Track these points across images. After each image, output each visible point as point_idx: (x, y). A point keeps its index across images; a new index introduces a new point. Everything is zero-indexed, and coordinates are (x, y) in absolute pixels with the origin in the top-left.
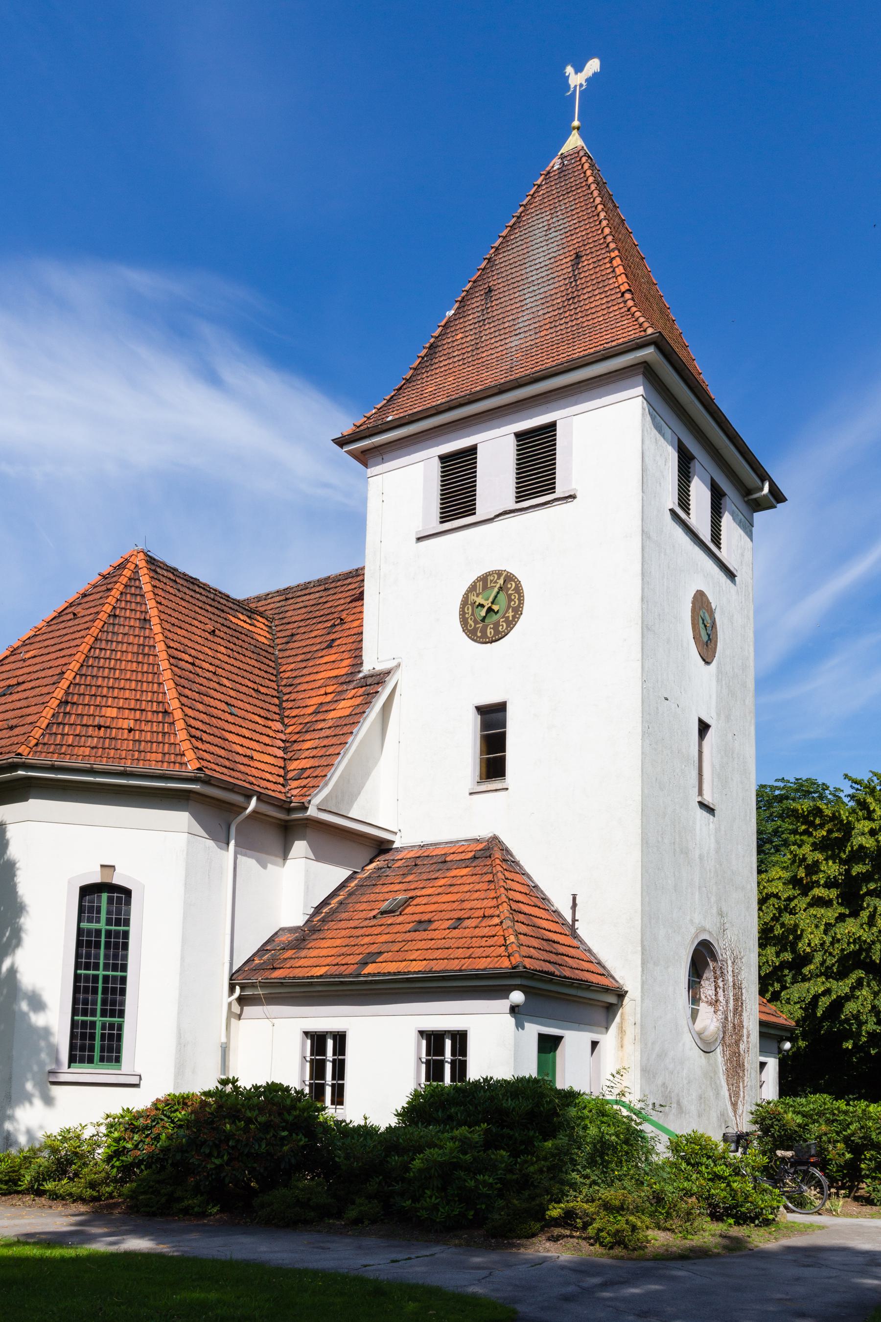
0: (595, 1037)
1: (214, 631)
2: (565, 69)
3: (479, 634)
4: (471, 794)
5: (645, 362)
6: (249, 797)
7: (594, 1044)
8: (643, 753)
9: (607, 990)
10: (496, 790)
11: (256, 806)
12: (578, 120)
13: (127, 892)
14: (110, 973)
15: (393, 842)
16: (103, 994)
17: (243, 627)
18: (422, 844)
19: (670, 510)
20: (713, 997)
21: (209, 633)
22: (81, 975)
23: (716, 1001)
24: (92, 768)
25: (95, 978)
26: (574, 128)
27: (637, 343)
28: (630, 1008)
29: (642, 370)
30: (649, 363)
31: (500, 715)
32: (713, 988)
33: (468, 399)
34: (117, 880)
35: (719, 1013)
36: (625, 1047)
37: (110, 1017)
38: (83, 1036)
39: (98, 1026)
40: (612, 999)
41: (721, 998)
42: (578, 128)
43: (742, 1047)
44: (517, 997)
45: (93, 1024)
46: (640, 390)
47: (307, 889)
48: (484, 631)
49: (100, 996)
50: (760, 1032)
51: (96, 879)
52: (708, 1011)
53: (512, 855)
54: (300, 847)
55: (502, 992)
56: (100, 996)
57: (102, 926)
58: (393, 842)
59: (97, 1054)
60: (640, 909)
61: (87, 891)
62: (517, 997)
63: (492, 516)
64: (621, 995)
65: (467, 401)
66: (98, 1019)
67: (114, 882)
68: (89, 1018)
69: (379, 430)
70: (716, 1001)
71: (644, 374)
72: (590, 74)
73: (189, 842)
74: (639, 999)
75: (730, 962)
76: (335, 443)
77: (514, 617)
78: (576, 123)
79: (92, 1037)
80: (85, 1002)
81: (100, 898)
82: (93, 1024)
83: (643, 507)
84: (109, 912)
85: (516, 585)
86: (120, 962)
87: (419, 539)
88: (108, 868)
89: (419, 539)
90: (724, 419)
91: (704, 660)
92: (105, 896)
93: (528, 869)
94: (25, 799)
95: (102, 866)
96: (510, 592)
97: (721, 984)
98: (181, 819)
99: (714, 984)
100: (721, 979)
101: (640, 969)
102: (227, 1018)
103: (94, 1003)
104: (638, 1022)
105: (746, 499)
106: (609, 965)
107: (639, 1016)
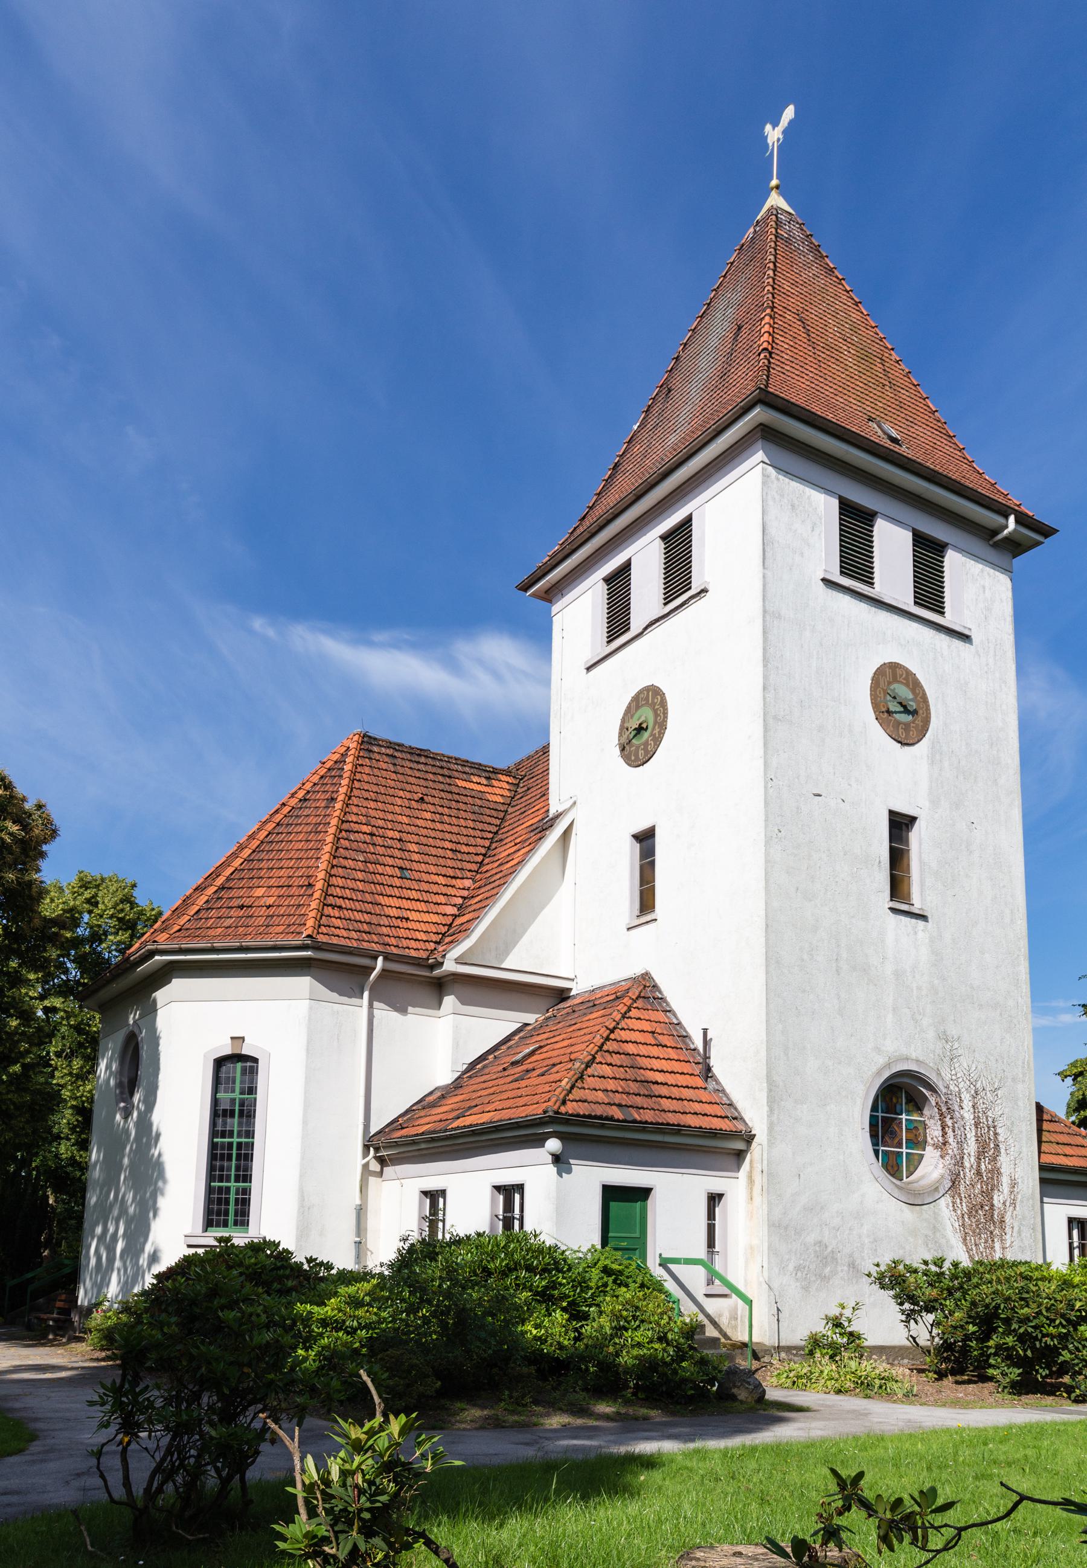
0: (716, 1189)
1: (422, 799)
2: (764, 129)
3: (633, 758)
4: (628, 929)
5: (761, 424)
6: (376, 958)
7: (714, 1199)
8: (767, 861)
9: (734, 1135)
10: (647, 922)
11: (383, 965)
12: (777, 178)
13: (255, 1060)
14: (243, 1140)
15: (570, 990)
16: (236, 1160)
17: (465, 788)
18: (592, 989)
19: (823, 580)
20: (940, 1139)
21: (417, 801)
22: (217, 1143)
23: (944, 1144)
24: (181, 948)
25: (230, 1144)
26: (772, 189)
27: (742, 408)
28: (756, 1153)
29: (759, 434)
30: (766, 423)
31: (649, 841)
32: (940, 1128)
33: (612, 513)
34: (245, 1051)
35: (948, 1157)
36: (754, 1199)
37: (243, 1182)
38: (219, 1201)
39: (233, 1191)
40: (740, 1145)
41: (951, 1140)
42: (777, 187)
43: (997, 1200)
44: (554, 1145)
45: (228, 1189)
46: (760, 455)
47: (456, 1045)
48: (636, 755)
49: (234, 1162)
50: (1040, 1178)
51: (228, 1051)
52: (933, 1155)
53: (660, 992)
54: (449, 1001)
55: (538, 1141)
56: (234, 1162)
57: (237, 1095)
58: (570, 990)
59: (231, 1218)
60: (765, 1039)
61: (220, 1063)
62: (554, 1145)
63: (640, 630)
64: (749, 1138)
65: (611, 516)
66: (232, 1184)
67: (243, 1052)
68: (224, 1184)
69: (549, 568)
70: (944, 1144)
71: (764, 438)
72: (786, 124)
73: (311, 1008)
74: (765, 1143)
75: (966, 1097)
76: (519, 589)
77: (660, 733)
78: (774, 182)
79: (227, 1202)
80: (222, 1169)
81: (235, 1068)
82: (228, 1189)
83: (764, 586)
84: (242, 1082)
85: (662, 698)
86: (904, 1150)
87: (589, 669)
88: (239, 1040)
89: (589, 669)
90: (906, 460)
91: (899, 742)
92: (239, 1065)
93: (674, 1005)
94: (170, 982)
95: (232, 1038)
96: (656, 707)
97: (949, 1123)
98: (304, 983)
99: (939, 1122)
100: (949, 1116)
101: (766, 1109)
102: (361, 1180)
103: (229, 1169)
104: (765, 1169)
105: (991, 543)
106: (740, 1105)
107: (765, 1162)
